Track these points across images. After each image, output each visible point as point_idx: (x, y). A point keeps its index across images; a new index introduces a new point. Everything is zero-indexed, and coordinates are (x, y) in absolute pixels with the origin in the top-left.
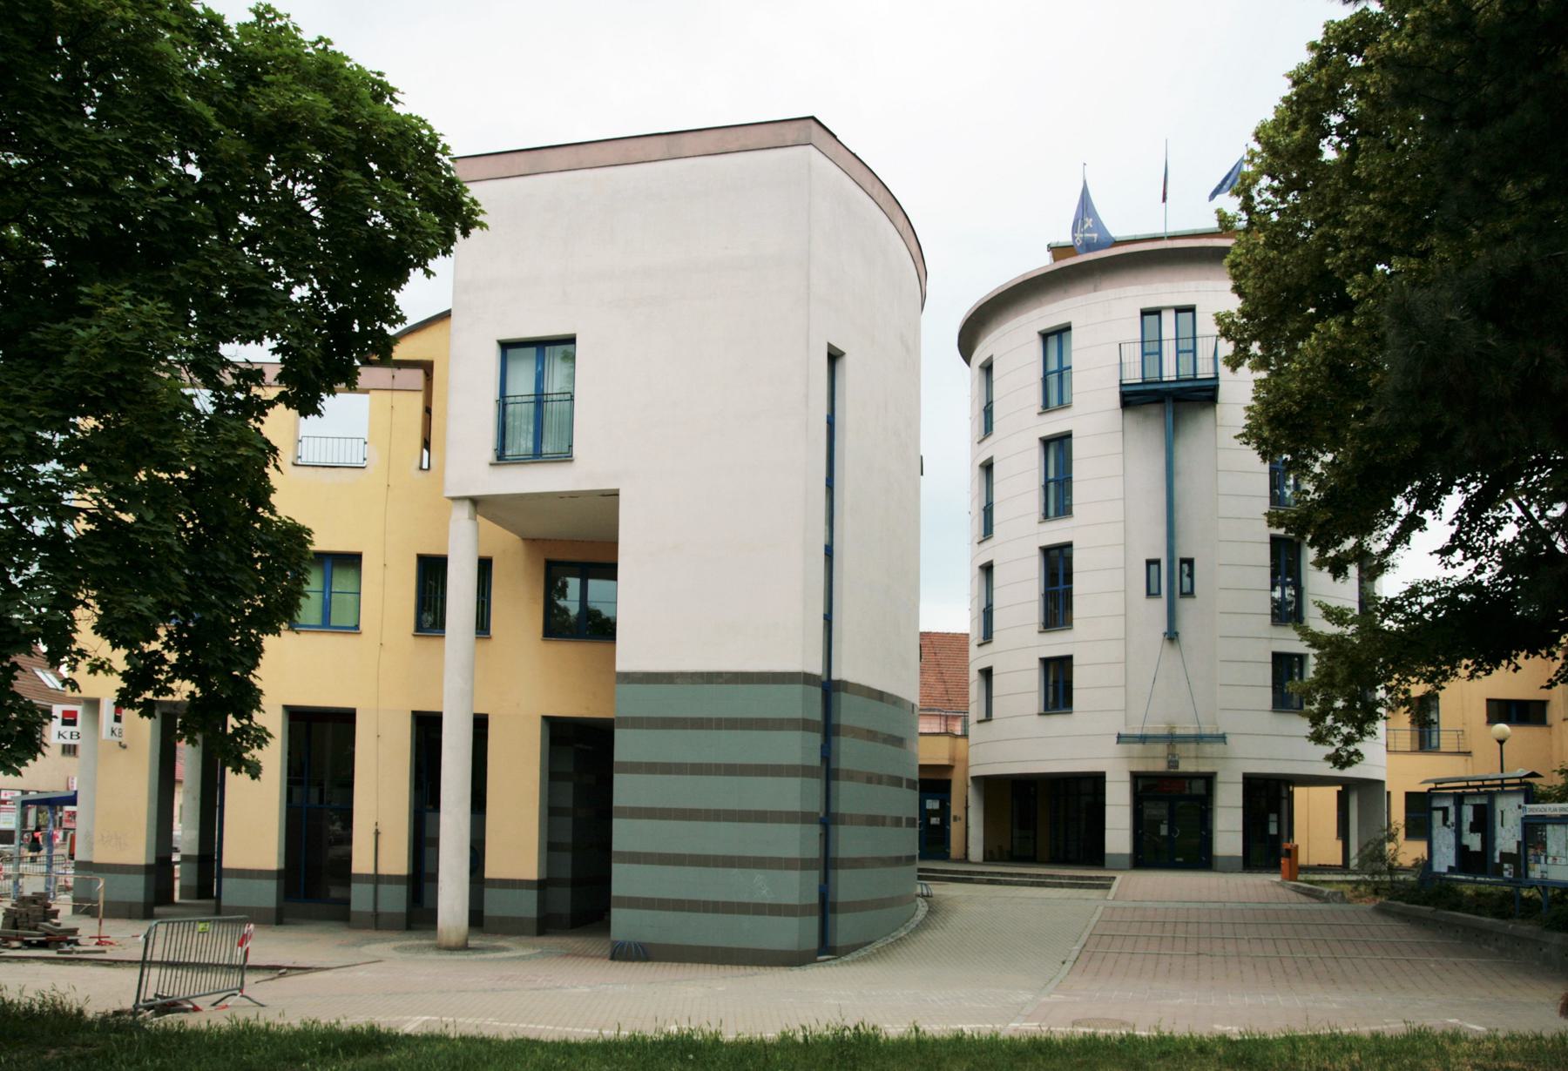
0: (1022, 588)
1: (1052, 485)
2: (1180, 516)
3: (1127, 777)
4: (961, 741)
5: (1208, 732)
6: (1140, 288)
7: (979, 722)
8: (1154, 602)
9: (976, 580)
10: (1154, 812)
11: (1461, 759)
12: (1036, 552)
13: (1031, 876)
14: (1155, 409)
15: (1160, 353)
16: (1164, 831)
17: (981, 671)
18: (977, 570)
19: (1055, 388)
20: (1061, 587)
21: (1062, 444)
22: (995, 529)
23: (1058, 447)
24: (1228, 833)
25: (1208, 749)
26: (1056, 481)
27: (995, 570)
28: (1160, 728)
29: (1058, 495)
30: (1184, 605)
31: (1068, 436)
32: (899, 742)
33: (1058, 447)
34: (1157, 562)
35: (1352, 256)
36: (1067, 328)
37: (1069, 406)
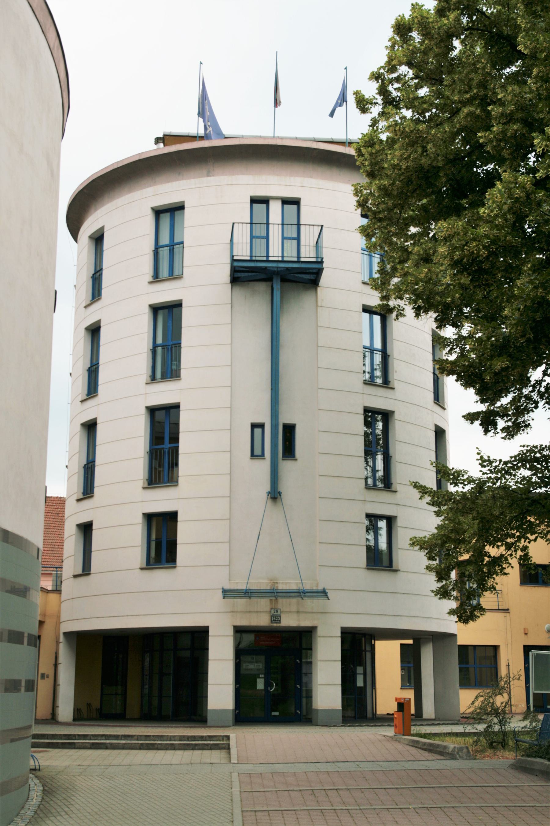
0: (126, 447)
1: (159, 350)
2: (283, 385)
3: (231, 632)
4: (53, 597)
5: (307, 587)
6: (251, 177)
7: (75, 576)
8: (257, 463)
9: (77, 439)
10: (251, 666)
11: (501, 615)
12: (143, 411)
13: (139, 737)
14: (262, 287)
15: (267, 238)
16: (260, 684)
17: (79, 526)
18: (78, 428)
19: (166, 259)
20: (167, 445)
21: (171, 313)
22: (100, 388)
23: (167, 314)
24: (326, 686)
25: (310, 603)
26: (163, 346)
27: (99, 428)
28: (264, 584)
29: (166, 360)
30: (286, 466)
31: (178, 305)
32: (22, 592)
33: (167, 314)
34: (261, 426)
35: (504, 132)
36: (181, 207)
37: (180, 277)
